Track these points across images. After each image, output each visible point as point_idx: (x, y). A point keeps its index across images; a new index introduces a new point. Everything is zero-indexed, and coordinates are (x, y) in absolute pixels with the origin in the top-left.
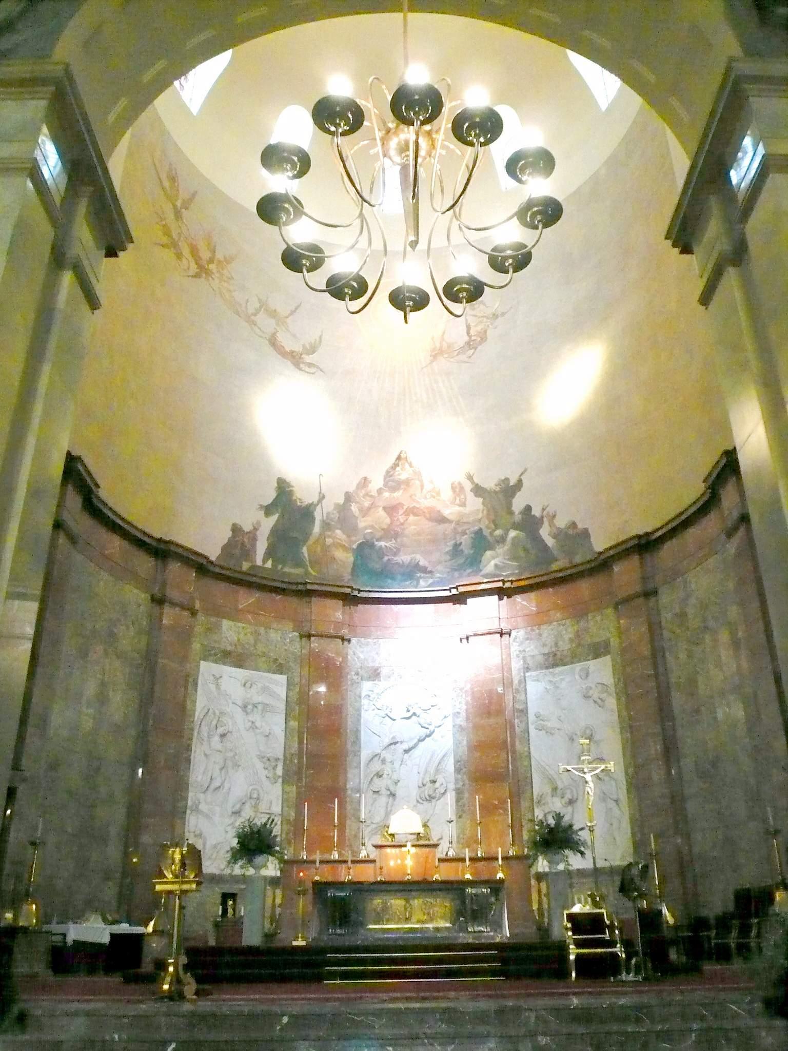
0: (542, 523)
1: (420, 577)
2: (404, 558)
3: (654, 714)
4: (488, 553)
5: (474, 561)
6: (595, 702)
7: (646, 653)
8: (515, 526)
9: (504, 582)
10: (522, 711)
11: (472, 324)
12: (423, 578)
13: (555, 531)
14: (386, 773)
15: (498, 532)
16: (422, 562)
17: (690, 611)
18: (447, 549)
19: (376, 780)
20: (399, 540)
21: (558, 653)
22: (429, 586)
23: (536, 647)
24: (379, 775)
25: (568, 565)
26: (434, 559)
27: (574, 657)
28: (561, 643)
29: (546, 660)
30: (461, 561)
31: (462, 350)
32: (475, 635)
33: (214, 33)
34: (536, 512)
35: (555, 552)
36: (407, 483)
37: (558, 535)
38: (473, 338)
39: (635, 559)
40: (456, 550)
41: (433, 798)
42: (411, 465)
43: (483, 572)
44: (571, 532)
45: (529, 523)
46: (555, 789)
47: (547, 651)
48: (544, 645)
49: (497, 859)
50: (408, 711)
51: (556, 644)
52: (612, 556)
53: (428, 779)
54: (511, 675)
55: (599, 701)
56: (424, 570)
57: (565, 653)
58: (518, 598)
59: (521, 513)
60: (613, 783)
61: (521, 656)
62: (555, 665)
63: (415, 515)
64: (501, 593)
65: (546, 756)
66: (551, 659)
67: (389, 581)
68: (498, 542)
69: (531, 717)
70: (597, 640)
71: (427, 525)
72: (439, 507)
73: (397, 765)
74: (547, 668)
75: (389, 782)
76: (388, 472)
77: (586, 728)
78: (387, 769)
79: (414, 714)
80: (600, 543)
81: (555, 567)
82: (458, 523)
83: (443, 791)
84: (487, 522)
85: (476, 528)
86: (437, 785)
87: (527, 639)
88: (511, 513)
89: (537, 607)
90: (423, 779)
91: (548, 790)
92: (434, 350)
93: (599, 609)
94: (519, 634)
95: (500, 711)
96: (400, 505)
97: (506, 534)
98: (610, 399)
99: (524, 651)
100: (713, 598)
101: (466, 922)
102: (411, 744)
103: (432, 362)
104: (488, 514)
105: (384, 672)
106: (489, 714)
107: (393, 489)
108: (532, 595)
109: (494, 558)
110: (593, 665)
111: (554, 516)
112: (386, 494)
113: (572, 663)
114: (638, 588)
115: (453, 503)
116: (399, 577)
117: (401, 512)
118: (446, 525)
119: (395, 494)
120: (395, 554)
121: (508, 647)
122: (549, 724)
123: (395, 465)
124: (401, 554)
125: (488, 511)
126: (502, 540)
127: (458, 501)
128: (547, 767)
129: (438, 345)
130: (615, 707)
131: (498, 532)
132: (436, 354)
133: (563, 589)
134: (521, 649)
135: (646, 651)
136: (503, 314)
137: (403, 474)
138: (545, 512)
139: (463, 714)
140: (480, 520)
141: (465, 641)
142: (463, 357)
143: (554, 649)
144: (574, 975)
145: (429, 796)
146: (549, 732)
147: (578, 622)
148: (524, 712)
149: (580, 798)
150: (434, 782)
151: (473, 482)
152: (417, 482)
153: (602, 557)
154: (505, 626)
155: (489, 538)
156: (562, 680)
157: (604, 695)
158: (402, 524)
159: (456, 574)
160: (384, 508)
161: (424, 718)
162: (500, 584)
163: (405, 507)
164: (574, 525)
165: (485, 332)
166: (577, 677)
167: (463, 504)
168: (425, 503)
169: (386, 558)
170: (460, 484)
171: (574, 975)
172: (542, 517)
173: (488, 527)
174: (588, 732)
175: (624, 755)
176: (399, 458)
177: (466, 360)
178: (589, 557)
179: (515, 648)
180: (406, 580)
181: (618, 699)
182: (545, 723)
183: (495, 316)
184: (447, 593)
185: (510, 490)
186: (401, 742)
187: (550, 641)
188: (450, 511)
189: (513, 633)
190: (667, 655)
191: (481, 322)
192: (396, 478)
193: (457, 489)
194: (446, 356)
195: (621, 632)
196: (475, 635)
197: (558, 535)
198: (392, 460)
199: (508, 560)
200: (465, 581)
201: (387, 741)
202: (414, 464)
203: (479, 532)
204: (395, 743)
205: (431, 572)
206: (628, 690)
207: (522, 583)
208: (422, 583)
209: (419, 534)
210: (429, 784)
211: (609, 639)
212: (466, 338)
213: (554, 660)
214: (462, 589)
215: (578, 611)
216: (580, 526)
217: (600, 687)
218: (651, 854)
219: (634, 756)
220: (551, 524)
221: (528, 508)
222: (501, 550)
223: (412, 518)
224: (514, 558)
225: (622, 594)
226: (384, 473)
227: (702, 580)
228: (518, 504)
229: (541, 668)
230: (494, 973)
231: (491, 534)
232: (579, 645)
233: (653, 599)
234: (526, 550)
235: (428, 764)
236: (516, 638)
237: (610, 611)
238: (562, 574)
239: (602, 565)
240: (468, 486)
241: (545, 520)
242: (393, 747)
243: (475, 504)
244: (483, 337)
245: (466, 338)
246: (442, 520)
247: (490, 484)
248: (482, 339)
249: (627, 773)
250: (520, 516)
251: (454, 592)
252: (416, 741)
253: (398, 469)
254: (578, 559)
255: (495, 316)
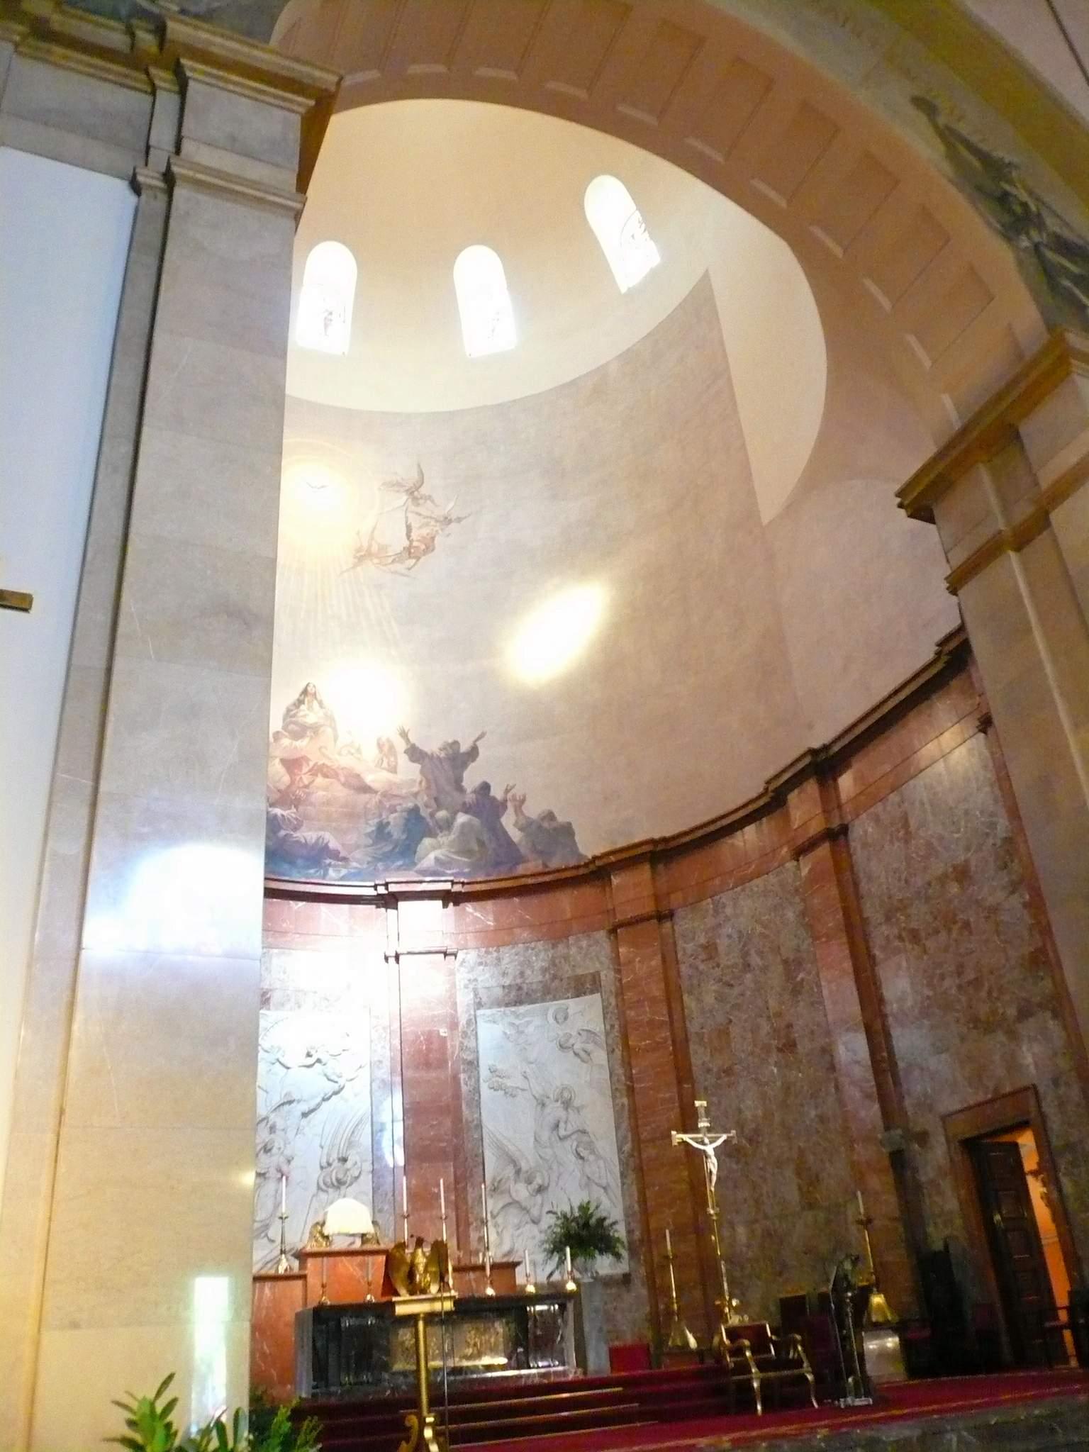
0: (505, 808)
1: (330, 865)
2: (308, 835)
3: (657, 1072)
4: (427, 841)
5: (407, 851)
6: (576, 1054)
7: (657, 993)
8: (467, 809)
9: (453, 883)
10: (470, 1063)
11: (415, 525)
12: (335, 866)
13: (522, 821)
14: (276, 1145)
15: (442, 814)
16: (333, 844)
17: (723, 944)
18: (369, 830)
19: (263, 1156)
20: (301, 808)
21: (525, 987)
22: (342, 879)
23: (492, 976)
24: (267, 1150)
25: (540, 869)
26: (350, 840)
27: (547, 993)
28: (528, 972)
29: (508, 994)
30: (389, 848)
31: (398, 558)
32: (409, 953)
33: (841, 256)
34: (497, 792)
35: (523, 850)
36: (315, 729)
37: (527, 826)
38: (415, 544)
39: (645, 872)
40: (381, 831)
41: (344, 1183)
42: (321, 704)
43: (418, 867)
44: (546, 825)
45: (486, 806)
46: (518, 1172)
47: (508, 983)
48: (504, 974)
49: (455, 1270)
50: (309, 1055)
51: (522, 974)
52: (613, 863)
53: (335, 1156)
54: (456, 1011)
55: (582, 1054)
56: (335, 855)
57: (534, 987)
58: (469, 907)
59: (474, 792)
60: (601, 1163)
61: (471, 986)
62: (518, 1002)
63: (325, 776)
64: (448, 898)
65: (505, 1125)
66: (513, 993)
67: (286, 866)
68: (441, 828)
69: (484, 1072)
70: (580, 972)
71: (341, 793)
72: (359, 768)
73: (291, 1134)
74: (507, 1005)
75: (282, 1159)
76: (289, 710)
77: (563, 1089)
78: (278, 1142)
79: (319, 1061)
80: (590, 845)
81: (521, 870)
82: (385, 795)
83: (356, 1174)
84: (426, 798)
85: (410, 805)
86: (349, 1164)
87: (481, 964)
88: (461, 790)
89: (496, 920)
90: (329, 1155)
91: (510, 1171)
92: (358, 550)
93: (588, 929)
94: (470, 956)
95: (442, 1063)
96: (305, 759)
97: (454, 818)
98: (610, 663)
99: (476, 980)
100: (759, 929)
101: (526, 1353)
102: (312, 1104)
103: (355, 566)
104: (428, 788)
105: (276, 997)
106: (428, 1065)
107: (297, 736)
108: (489, 905)
109: (434, 848)
110: (573, 1005)
111: (523, 801)
112: (286, 742)
113: (543, 1000)
114: (648, 907)
115: (379, 764)
116: (300, 862)
117: (305, 769)
118: (368, 796)
119: (298, 743)
120: (295, 829)
121: (452, 973)
122: (509, 1083)
123: (300, 702)
124: (303, 828)
125: (428, 781)
126: (448, 825)
127: (385, 765)
128: (505, 1142)
129: (365, 545)
130: (605, 1063)
131: (442, 814)
132: (363, 556)
133: (534, 901)
134: (471, 976)
135: (657, 990)
136: (459, 520)
137: (310, 715)
138: (509, 796)
139: (387, 1063)
140: (416, 795)
141: (392, 960)
142: (399, 567)
143: (519, 981)
144: (759, 1407)
145: (338, 1181)
146: (510, 1093)
147: (554, 946)
148: (473, 1065)
149: (553, 1184)
150: (344, 1160)
151: (408, 741)
152: (329, 730)
153: (598, 863)
154: (450, 945)
155: (428, 820)
156: (528, 1023)
157: (590, 1047)
158: (306, 787)
159: (380, 866)
160: (283, 761)
161: (332, 1067)
162: (447, 886)
163: (311, 764)
164: (550, 816)
165: (433, 538)
166: (551, 1020)
167: (393, 770)
168: (343, 761)
169: (282, 833)
170: (388, 740)
171: (759, 1407)
172: (506, 801)
173: (427, 806)
174: (566, 1095)
175: (617, 1128)
176: (305, 692)
177: (404, 571)
178: (572, 863)
179: (462, 976)
180: (309, 867)
181: (611, 1052)
182: (505, 1081)
183: (447, 521)
184: (371, 892)
185: (459, 758)
186: (299, 1101)
187: (512, 969)
188: (376, 778)
189: (461, 955)
190: (685, 997)
191: (427, 525)
192: (300, 720)
193: (385, 749)
194: (376, 561)
195: (618, 965)
196: (409, 953)
197: (527, 826)
198: (295, 695)
199: (457, 853)
200: (397, 880)
201: (277, 1100)
202: (325, 703)
203: (414, 811)
204: (290, 1102)
205: (344, 859)
206: (625, 1040)
207: (478, 887)
208: (331, 872)
209: (328, 803)
210: (336, 1164)
211: (598, 973)
212: (406, 543)
213: (517, 996)
214: (393, 888)
215: (556, 933)
216: (561, 818)
217: (584, 1034)
218: (667, 1257)
219: (635, 1130)
220: (518, 810)
221: (485, 787)
222: (445, 839)
223: (320, 780)
224: (467, 852)
225: (629, 913)
226: (283, 710)
227: (748, 910)
228: (472, 778)
229: (499, 1005)
230: (641, 1416)
231: (432, 815)
232: (554, 977)
233: (668, 924)
234: (481, 843)
235: (336, 1132)
236: (464, 961)
237: (601, 935)
238: (536, 883)
239: (596, 873)
240: (401, 746)
241: (509, 804)
242: (287, 1107)
243: (409, 772)
244: (429, 547)
245: (406, 543)
246: (365, 789)
247: (433, 746)
248: (427, 548)
249: (620, 1150)
250: (474, 796)
251: (382, 890)
252: (319, 1099)
253: (303, 707)
254: (555, 863)
255: (447, 521)
